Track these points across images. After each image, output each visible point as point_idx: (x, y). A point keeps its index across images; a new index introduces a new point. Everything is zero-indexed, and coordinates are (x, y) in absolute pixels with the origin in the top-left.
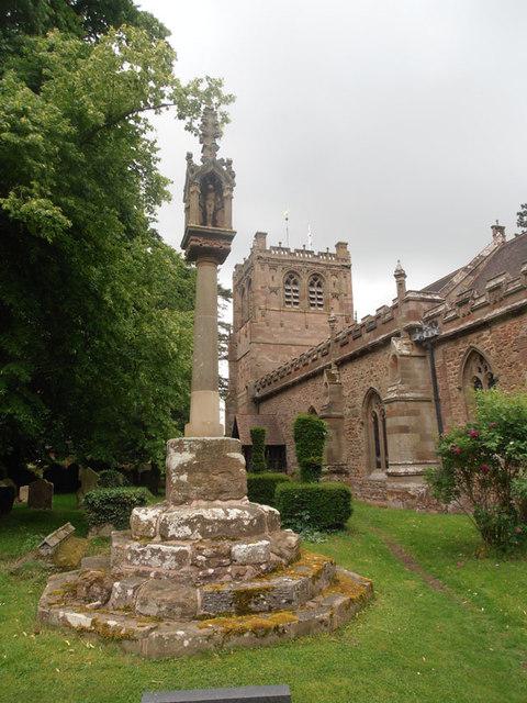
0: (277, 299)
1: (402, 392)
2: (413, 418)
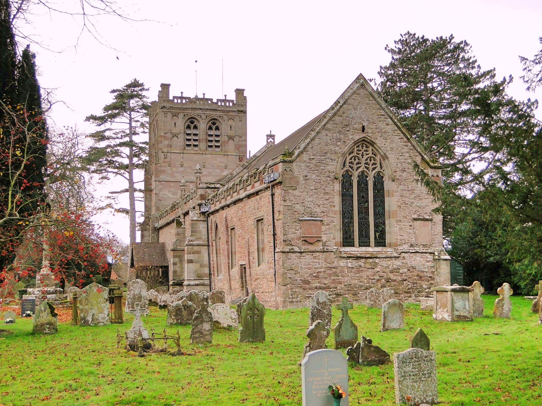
0: (180, 141)
1: (191, 241)
2: (196, 255)
